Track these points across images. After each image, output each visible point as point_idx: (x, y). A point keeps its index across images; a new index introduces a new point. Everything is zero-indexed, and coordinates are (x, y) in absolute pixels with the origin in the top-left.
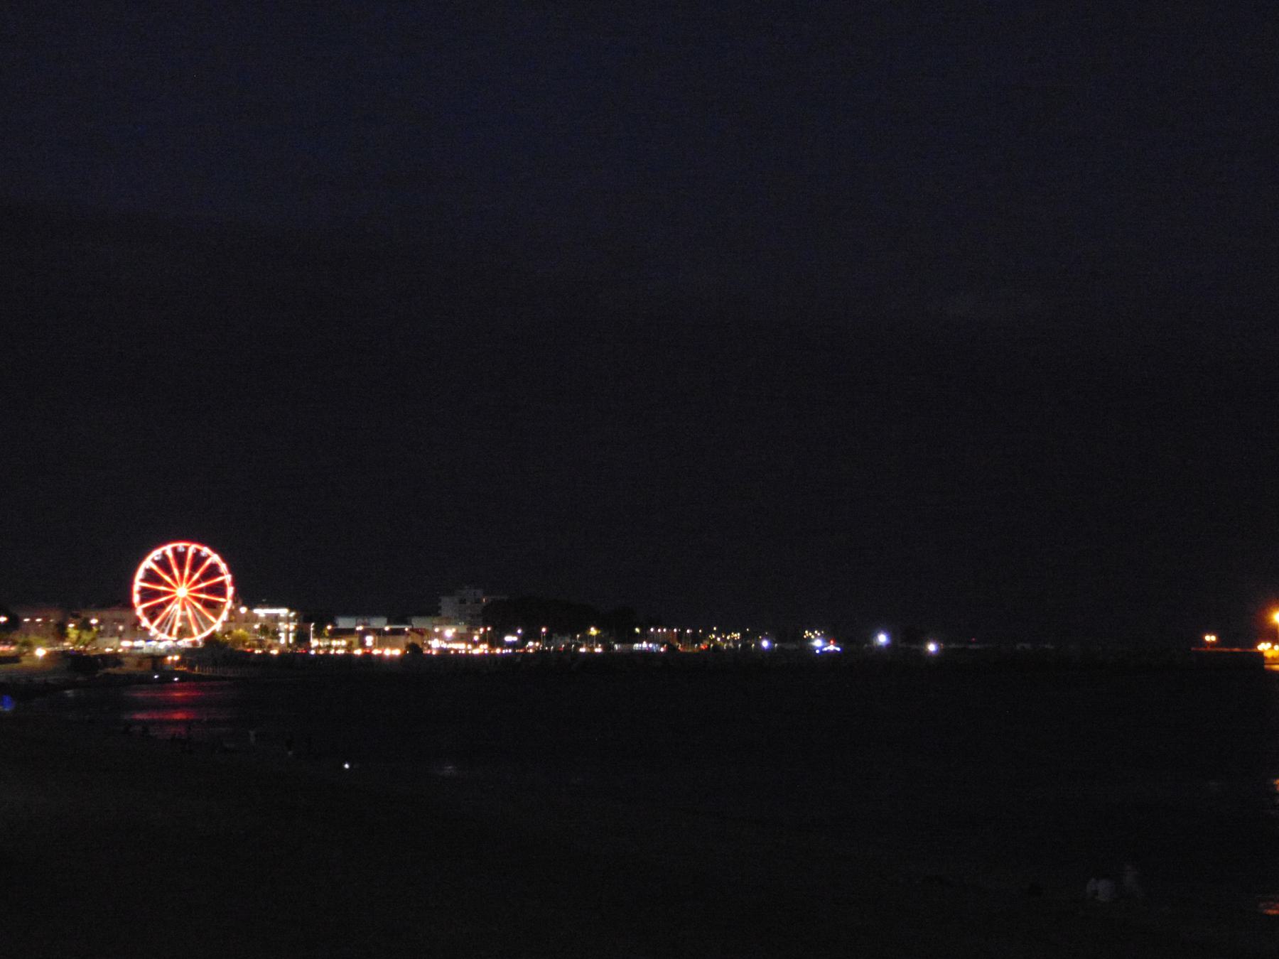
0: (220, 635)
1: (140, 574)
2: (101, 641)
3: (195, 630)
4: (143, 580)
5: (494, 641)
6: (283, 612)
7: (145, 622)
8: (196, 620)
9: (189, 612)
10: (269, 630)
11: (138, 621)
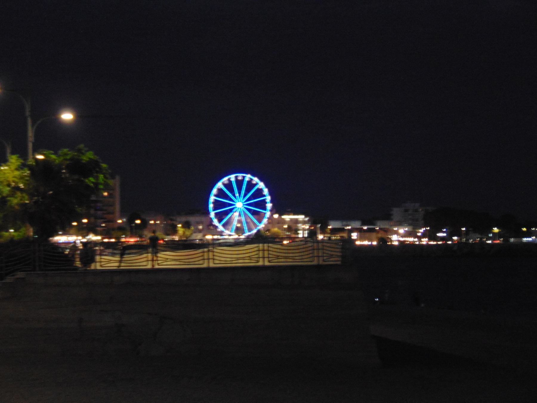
0: (263, 231)
1: (214, 191)
2: (194, 235)
3: (246, 228)
4: (215, 196)
5: (431, 236)
6: (301, 217)
7: (215, 222)
8: (247, 223)
9: (243, 218)
10: (293, 228)
11: (211, 220)
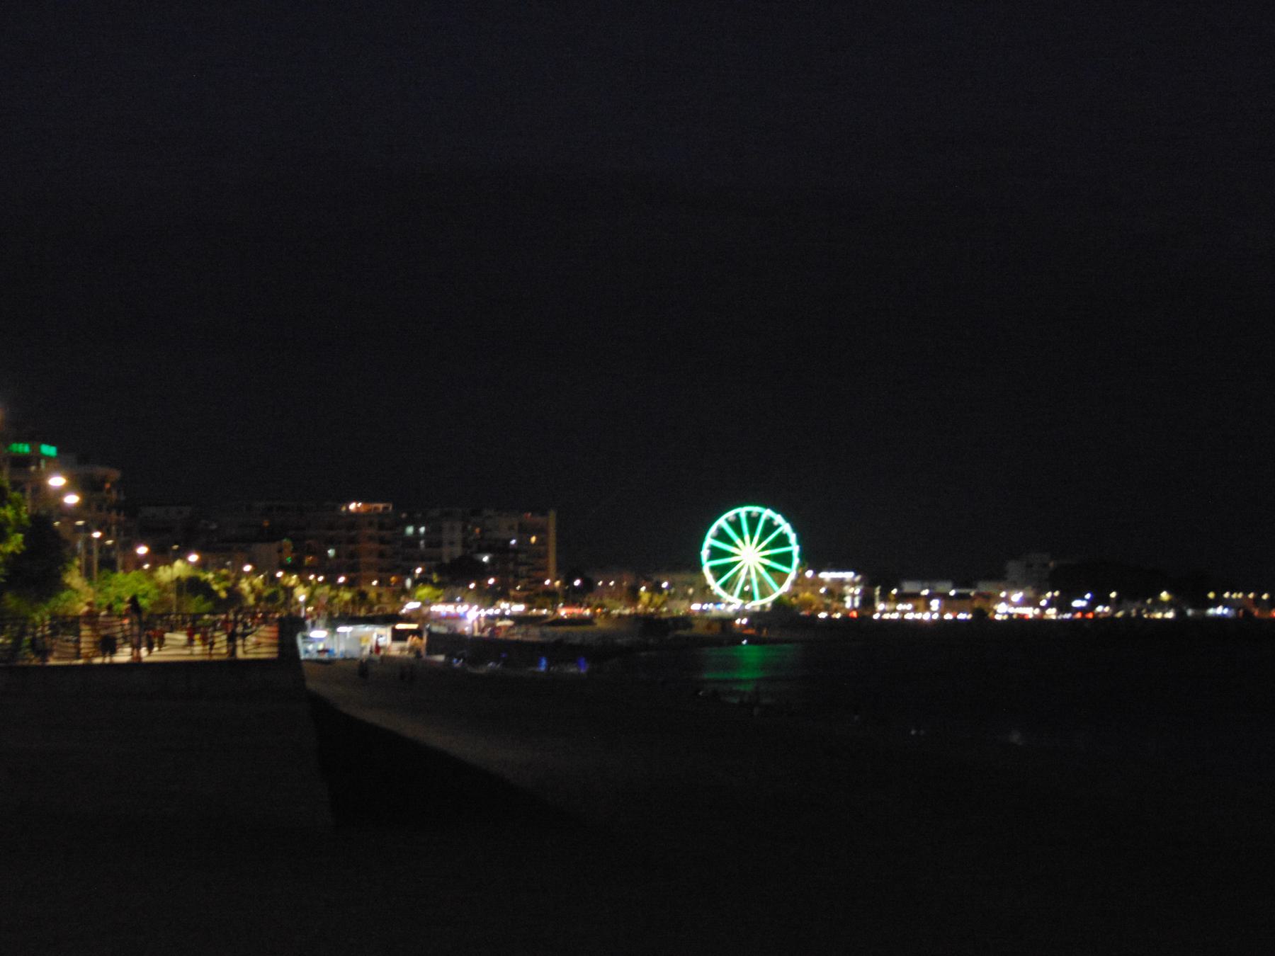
0: (786, 598)
5: (1063, 605)
6: (849, 575)
10: (836, 592)
